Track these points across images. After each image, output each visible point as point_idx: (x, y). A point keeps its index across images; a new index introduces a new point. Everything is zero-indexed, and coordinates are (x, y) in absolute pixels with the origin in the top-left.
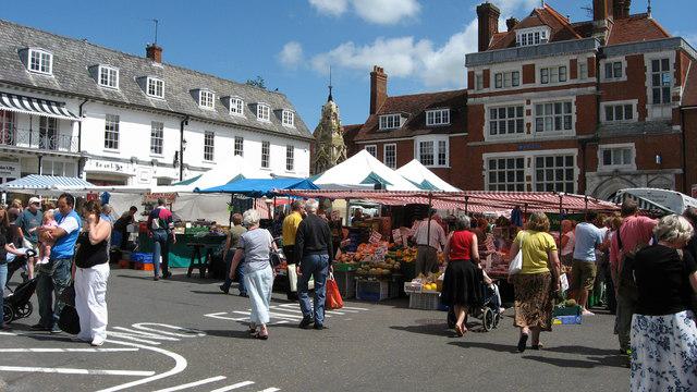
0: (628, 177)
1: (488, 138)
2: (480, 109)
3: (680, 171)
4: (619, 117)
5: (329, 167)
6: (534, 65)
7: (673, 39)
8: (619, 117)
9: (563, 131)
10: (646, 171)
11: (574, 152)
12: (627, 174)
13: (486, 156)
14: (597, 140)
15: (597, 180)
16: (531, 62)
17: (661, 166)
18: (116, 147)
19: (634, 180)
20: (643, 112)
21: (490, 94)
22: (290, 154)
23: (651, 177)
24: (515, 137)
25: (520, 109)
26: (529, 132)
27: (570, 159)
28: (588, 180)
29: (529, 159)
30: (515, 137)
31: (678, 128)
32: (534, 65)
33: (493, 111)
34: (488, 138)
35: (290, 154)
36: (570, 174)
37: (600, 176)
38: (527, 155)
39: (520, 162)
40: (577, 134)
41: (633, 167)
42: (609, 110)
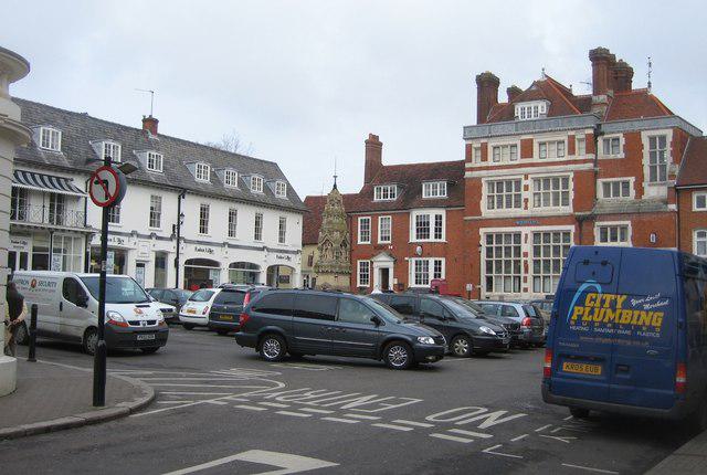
1: (486, 212)
2: (477, 183)
6: (532, 140)
11: (572, 228)
13: (482, 231)
14: (592, 219)
20: (640, 191)
21: (488, 168)
22: (232, 215)
25: (518, 182)
26: (526, 208)
34: (486, 212)
38: (526, 230)
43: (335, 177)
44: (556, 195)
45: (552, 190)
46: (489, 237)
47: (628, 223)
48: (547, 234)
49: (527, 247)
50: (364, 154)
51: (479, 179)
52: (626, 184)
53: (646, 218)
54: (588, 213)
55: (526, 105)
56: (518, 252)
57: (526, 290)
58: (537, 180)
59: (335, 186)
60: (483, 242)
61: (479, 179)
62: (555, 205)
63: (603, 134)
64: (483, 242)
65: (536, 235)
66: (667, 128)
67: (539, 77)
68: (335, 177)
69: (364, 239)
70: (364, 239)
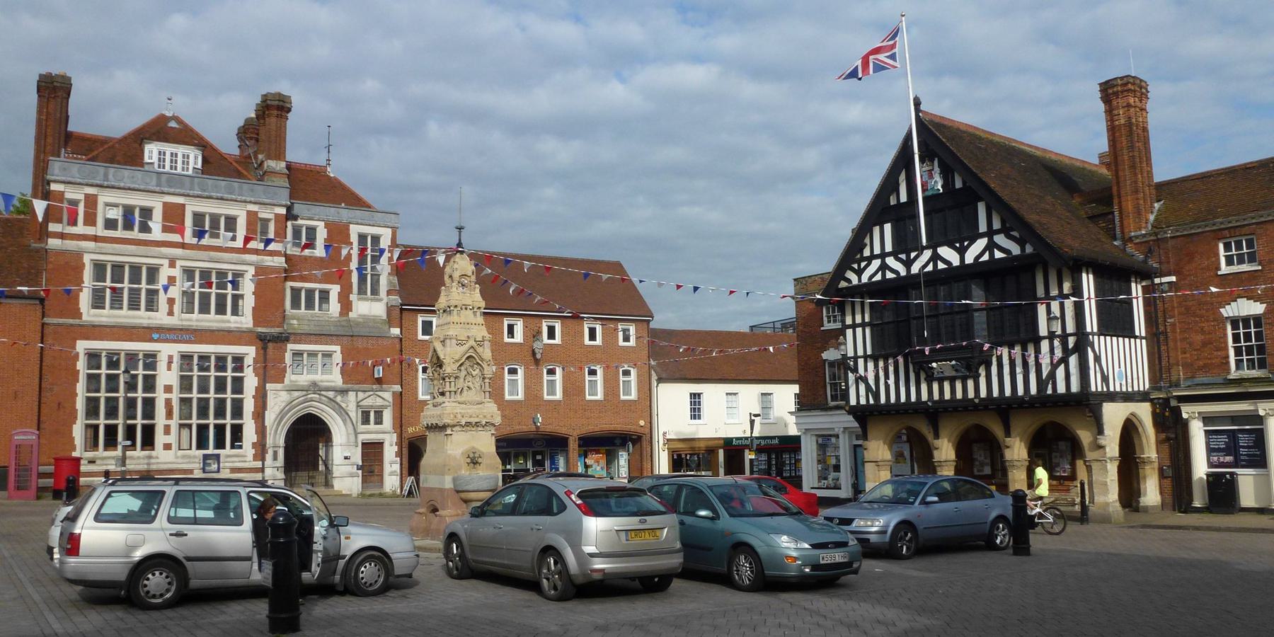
0: (331, 394)
1: (88, 314)
2: (73, 265)
3: (397, 388)
4: (310, 305)
5: (485, 516)
6: (183, 206)
7: (1113, 141)
8: (310, 305)
9: (229, 316)
10: (356, 387)
11: (250, 352)
12: (328, 389)
13: (82, 346)
14: (283, 339)
15: (284, 396)
16: (180, 200)
17: (379, 381)
18: (699, 418)
19: (339, 399)
20: (346, 306)
21: (95, 239)
22: (1111, 339)
23: (361, 395)
24: (125, 316)
25: (153, 272)
26: (171, 313)
27: (239, 361)
28: (270, 396)
29: (171, 357)
30: (142, 317)
31: (396, 331)
32: (183, 206)
33: (99, 268)
34: (88, 314)
35: (1111, 339)
36: (238, 385)
37: (290, 390)
38: (167, 350)
39: (151, 360)
40: (255, 324)
41: (336, 378)
42: (296, 293)
43: (460, 229)
44: (134, 294)
45: (108, 283)
46: (93, 357)
47: (337, 348)
48: (204, 358)
49: (167, 376)
50: (1238, 163)
51: (79, 255)
52: (325, 296)
53: (360, 344)
54: (278, 330)
55: (169, 148)
56: (150, 384)
57: (167, 447)
58: (189, 273)
59: (460, 240)
60: (81, 365)
61: (79, 255)
62: (201, 311)
63: (295, 218)
64: (81, 365)
65: (187, 358)
66: (319, 220)
67: (1098, 88)
68: (460, 229)
69: (511, 393)
70: (511, 393)
